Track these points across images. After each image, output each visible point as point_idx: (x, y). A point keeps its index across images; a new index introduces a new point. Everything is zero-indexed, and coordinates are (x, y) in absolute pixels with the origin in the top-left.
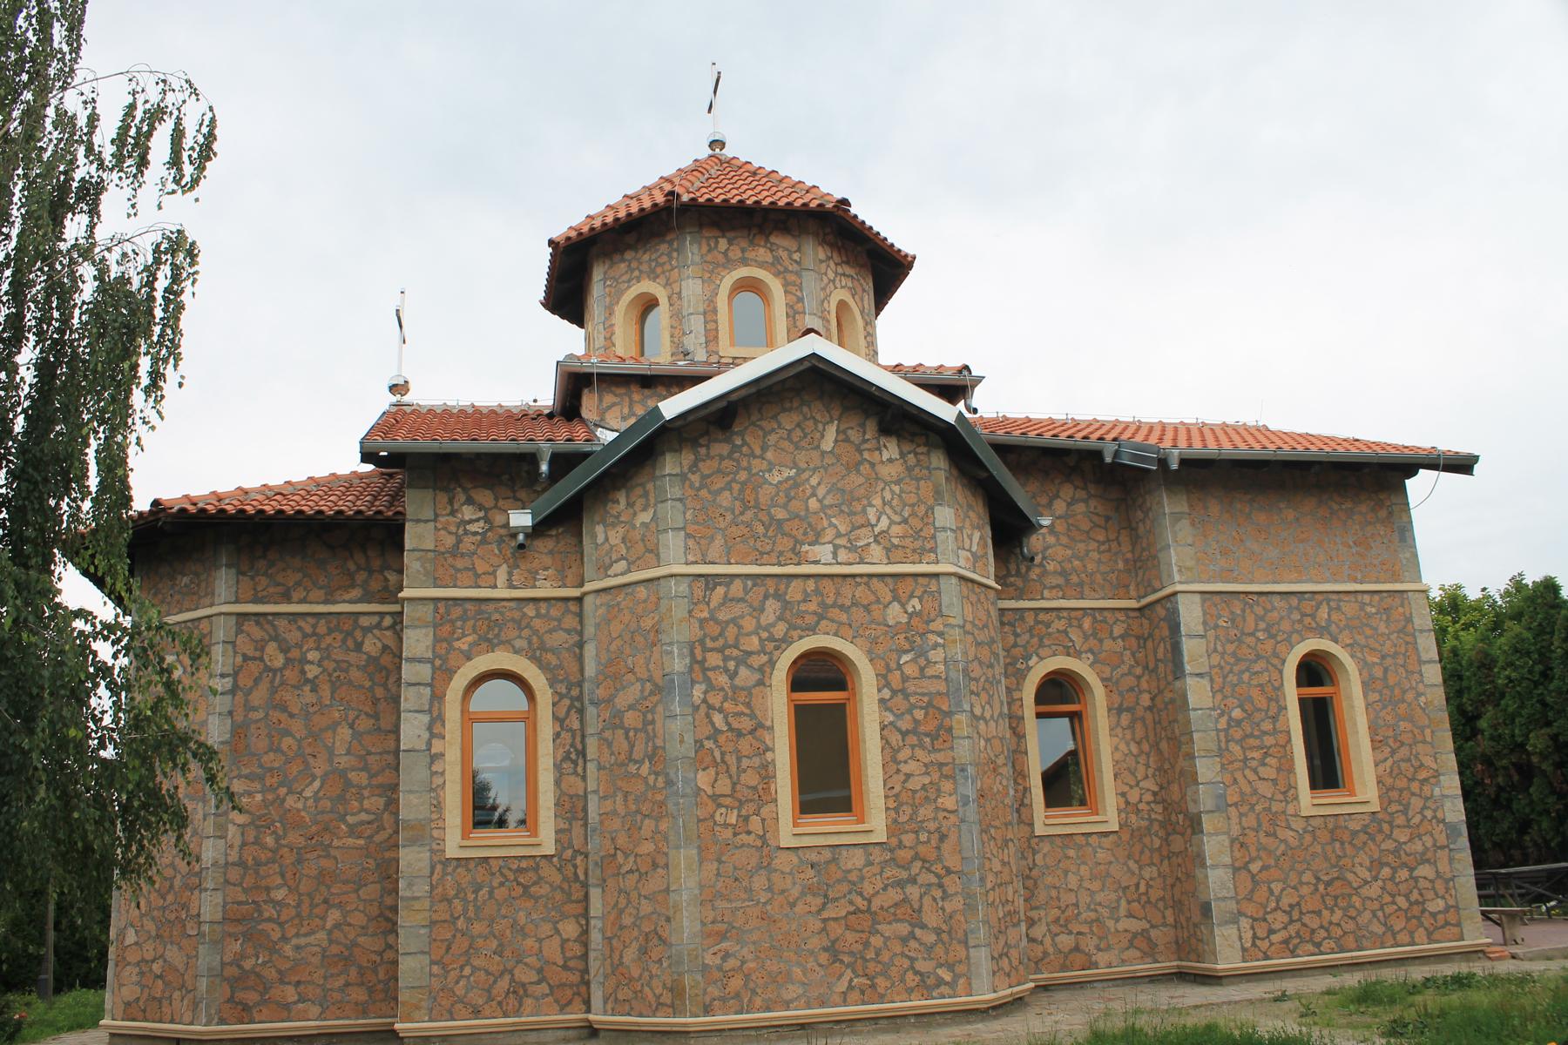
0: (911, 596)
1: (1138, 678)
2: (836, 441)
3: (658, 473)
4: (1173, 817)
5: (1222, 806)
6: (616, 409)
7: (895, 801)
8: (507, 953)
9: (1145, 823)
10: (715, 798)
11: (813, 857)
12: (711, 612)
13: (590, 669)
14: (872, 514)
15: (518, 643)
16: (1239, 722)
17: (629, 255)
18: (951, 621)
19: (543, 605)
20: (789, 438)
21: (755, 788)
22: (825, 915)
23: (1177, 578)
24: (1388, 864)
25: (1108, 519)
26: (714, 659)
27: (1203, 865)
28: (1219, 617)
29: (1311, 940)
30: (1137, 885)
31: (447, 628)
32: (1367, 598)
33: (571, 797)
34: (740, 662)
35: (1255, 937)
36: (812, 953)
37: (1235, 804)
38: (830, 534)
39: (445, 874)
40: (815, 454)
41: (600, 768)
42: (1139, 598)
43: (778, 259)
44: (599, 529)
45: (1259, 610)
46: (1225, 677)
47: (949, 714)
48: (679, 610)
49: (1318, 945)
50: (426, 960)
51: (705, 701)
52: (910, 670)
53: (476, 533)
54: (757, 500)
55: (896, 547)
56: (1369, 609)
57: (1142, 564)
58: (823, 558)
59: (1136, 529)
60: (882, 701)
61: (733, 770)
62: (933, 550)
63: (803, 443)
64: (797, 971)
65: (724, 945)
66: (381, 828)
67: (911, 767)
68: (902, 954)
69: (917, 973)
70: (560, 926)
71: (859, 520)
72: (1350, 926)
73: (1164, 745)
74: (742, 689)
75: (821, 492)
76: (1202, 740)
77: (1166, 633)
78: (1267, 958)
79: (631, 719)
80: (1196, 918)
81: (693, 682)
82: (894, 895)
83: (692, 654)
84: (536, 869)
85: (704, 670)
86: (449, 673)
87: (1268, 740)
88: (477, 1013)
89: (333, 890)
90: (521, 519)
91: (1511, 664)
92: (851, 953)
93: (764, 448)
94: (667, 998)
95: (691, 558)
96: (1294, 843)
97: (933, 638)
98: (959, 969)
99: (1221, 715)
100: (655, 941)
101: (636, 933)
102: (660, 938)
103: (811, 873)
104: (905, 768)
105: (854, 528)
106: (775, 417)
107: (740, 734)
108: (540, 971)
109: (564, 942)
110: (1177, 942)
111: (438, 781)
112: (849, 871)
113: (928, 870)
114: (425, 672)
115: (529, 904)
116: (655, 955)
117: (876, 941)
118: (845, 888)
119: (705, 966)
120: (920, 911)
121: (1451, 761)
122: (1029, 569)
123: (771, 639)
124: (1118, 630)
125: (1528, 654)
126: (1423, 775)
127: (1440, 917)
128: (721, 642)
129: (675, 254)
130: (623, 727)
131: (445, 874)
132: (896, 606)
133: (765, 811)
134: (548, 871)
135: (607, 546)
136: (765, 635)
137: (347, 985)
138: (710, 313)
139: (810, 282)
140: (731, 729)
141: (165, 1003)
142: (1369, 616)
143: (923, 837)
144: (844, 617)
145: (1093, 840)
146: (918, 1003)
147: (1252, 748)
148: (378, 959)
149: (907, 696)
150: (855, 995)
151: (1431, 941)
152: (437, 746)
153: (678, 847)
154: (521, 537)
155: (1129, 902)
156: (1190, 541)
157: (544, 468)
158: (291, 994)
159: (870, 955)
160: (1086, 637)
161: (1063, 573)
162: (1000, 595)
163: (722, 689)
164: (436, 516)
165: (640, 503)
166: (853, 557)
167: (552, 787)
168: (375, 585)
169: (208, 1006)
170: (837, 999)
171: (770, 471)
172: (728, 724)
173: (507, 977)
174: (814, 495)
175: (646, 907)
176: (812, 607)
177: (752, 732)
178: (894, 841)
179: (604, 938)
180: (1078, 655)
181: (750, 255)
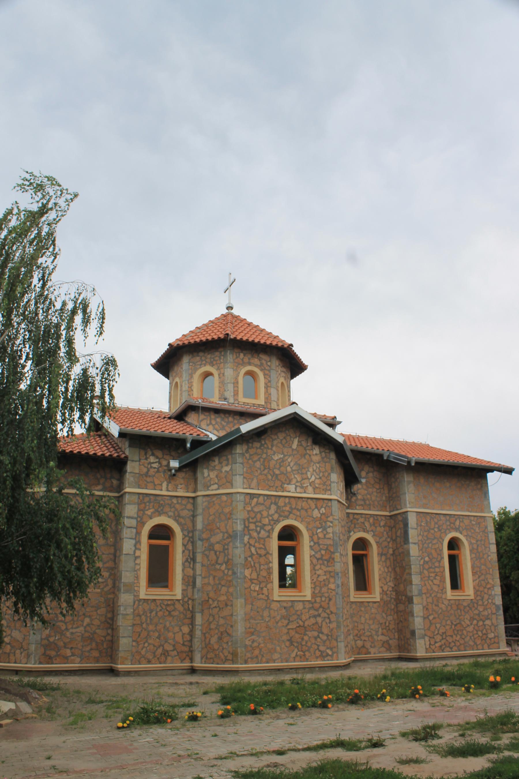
0: (322, 507)
1: (389, 542)
2: (298, 445)
3: (233, 452)
4: (400, 597)
5: (420, 594)
6: (205, 421)
7: (314, 585)
8: (162, 638)
9: (389, 599)
10: (251, 580)
11: (285, 604)
12: (252, 508)
13: (199, 526)
14: (309, 474)
15: (170, 514)
16: (427, 562)
17: (201, 354)
18: (335, 517)
19: (180, 499)
20: (281, 443)
21: (265, 577)
22: (289, 627)
23: (408, 505)
24: (475, 619)
25: (380, 480)
26: (252, 526)
27: (413, 615)
28: (422, 522)
29: (449, 647)
30: (385, 623)
31: (143, 505)
32: (472, 518)
33: (188, 576)
35: (430, 644)
36: (283, 641)
37: (425, 593)
38: (294, 481)
39: (139, 605)
41: (203, 565)
42: (390, 511)
43: (262, 364)
44: (206, 471)
45: (436, 520)
46: (423, 545)
47: (333, 553)
48: (240, 506)
49: (451, 648)
50: (130, 639)
51: (248, 542)
52: (321, 535)
53: (155, 468)
54: (269, 466)
55: (317, 488)
56: (474, 523)
57: (393, 498)
58: (291, 490)
60: (311, 547)
61: (258, 569)
62: (330, 490)
63: (286, 445)
64: (278, 648)
65: (253, 637)
66: (107, 585)
67: (319, 572)
68: (315, 644)
69: (320, 651)
70: (182, 628)
72: (462, 642)
73: (398, 569)
74: (262, 538)
75: (292, 464)
76: (414, 569)
77: (402, 526)
78: (434, 652)
79: (217, 547)
80: (408, 635)
81: (245, 535)
82: (313, 620)
83: (245, 524)
84: (174, 605)
85: (249, 530)
86: (143, 524)
87: (437, 570)
88: (149, 662)
89: (87, 610)
90: (175, 464)
91: (506, 544)
92: (297, 642)
93: (272, 446)
94: (230, 657)
95: (245, 486)
96: (444, 609)
97: (329, 524)
99: (421, 559)
100: (226, 635)
101: (217, 631)
102: (228, 633)
103: (284, 611)
104: (318, 573)
105: (303, 479)
106: (276, 434)
107: (260, 556)
108: (174, 646)
109: (183, 634)
110: (399, 646)
111: (137, 567)
112: (297, 611)
113: (325, 612)
114: (134, 523)
115: (171, 619)
116: (225, 640)
117: (306, 638)
118: (295, 617)
119: (246, 645)
120: (321, 627)
121: (498, 581)
122: (352, 497)
123: (273, 520)
124: (382, 523)
125: (513, 541)
126: (488, 586)
127: (492, 640)
128: (254, 520)
129: (222, 357)
130: (214, 550)
131: (139, 605)
132: (316, 510)
133: (269, 586)
134: (178, 606)
135: (209, 478)
136: (271, 518)
137: (91, 649)
138: (236, 383)
139: (273, 375)
140: (257, 554)
141: (11, 655)
142: (473, 525)
143: (323, 599)
144: (298, 513)
145: (371, 604)
146: (320, 662)
147: (431, 572)
148: (104, 639)
149: (319, 545)
150: (298, 658)
151: (489, 649)
152: (138, 553)
153: (237, 598)
154: (173, 471)
155: (382, 629)
156: (413, 492)
157: (188, 445)
158: (68, 652)
159: (304, 643)
160: (371, 525)
161: (364, 500)
162: (348, 508)
163: (255, 538)
164: (140, 459)
165: (225, 463)
166: (302, 490)
167: (181, 572)
168: (108, 484)
169: (35, 657)
170: (292, 659)
171: (274, 455)
172: (256, 552)
173: (161, 648)
174: (289, 465)
175: (222, 622)
177: (265, 555)
178: (313, 600)
179: (202, 633)
180: (367, 532)
181: (252, 361)
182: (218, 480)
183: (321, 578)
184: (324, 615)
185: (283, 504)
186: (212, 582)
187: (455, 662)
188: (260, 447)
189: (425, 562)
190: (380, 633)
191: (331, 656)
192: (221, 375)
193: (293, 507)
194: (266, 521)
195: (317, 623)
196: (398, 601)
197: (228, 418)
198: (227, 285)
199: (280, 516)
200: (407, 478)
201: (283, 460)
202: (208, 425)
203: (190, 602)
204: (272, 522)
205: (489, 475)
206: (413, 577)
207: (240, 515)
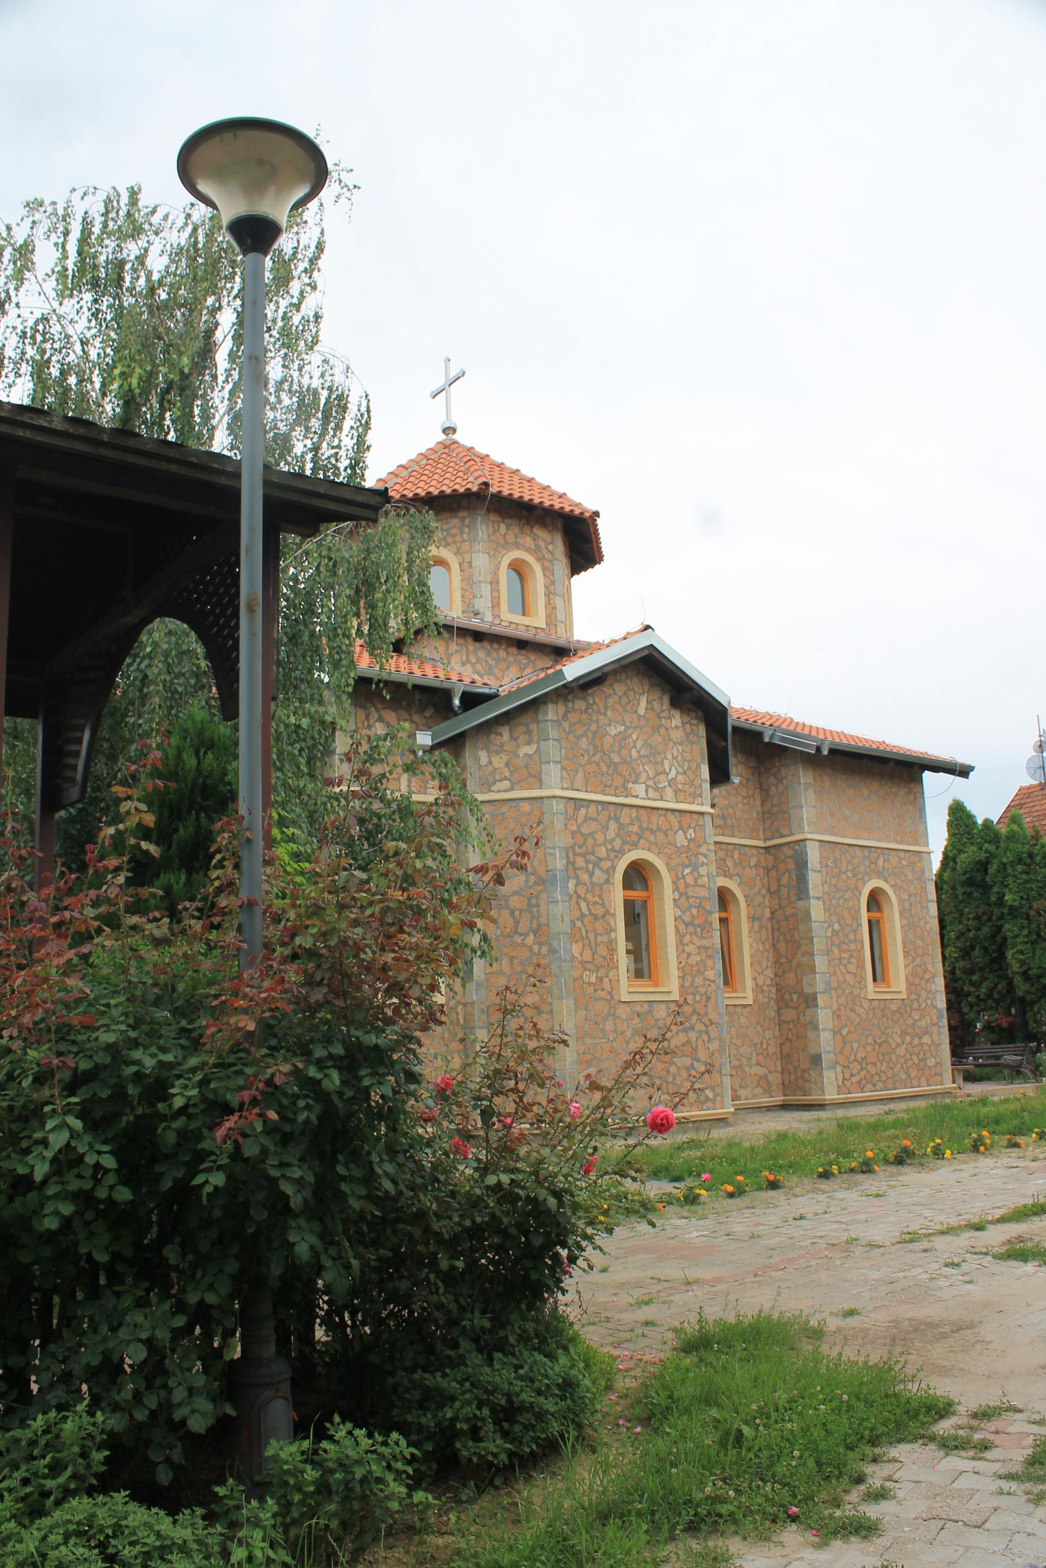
3: (540, 717)
4: (787, 996)
5: (827, 991)
6: (458, 655)
7: (684, 971)
10: (583, 963)
11: (638, 1008)
12: (578, 826)
21: (604, 957)
25: (748, 780)
26: (580, 862)
27: (816, 1028)
34: (596, 865)
38: (643, 777)
40: (634, 716)
42: (765, 840)
43: (538, 547)
44: (483, 755)
48: (559, 823)
49: (874, 1085)
51: (575, 892)
52: (690, 880)
57: (774, 814)
58: (640, 795)
59: (767, 791)
71: (660, 768)
72: (890, 1074)
73: (782, 947)
75: (639, 744)
76: (819, 944)
77: (792, 866)
80: (805, 1064)
81: (569, 878)
83: (568, 858)
87: (852, 946)
90: (424, 739)
92: (660, 1078)
93: (606, 708)
96: (864, 1016)
97: (702, 859)
98: (718, 1090)
103: (637, 1020)
104: (688, 949)
105: (658, 774)
107: (596, 918)
117: (673, 1069)
120: (696, 1049)
124: (753, 861)
126: (927, 976)
128: (583, 850)
129: (466, 530)
130: (508, 908)
135: (490, 768)
136: (609, 847)
138: (495, 583)
140: (591, 914)
153: (561, 998)
159: (670, 1079)
160: (735, 865)
165: (522, 738)
166: (656, 795)
174: (634, 747)
176: (635, 829)
181: (521, 541)
182: (511, 773)
183: (694, 959)
184: (700, 1027)
185: (627, 821)
186: (507, 969)
187: (903, 1105)
188: (587, 709)
189: (835, 933)
190: (754, 1061)
191: (713, 1101)
192: (466, 566)
193: (645, 826)
194: (602, 852)
195: (689, 1042)
196: (782, 1003)
197: (497, 650)
198: (441, 382)
199: (624, 842)
200: (805, 777)
201: (623, 737)
202: (463, 664)
203: (460, 1008)
204: (612, 855)
205: (927, 775)
206: (816, 958)
207: (558, 839)
